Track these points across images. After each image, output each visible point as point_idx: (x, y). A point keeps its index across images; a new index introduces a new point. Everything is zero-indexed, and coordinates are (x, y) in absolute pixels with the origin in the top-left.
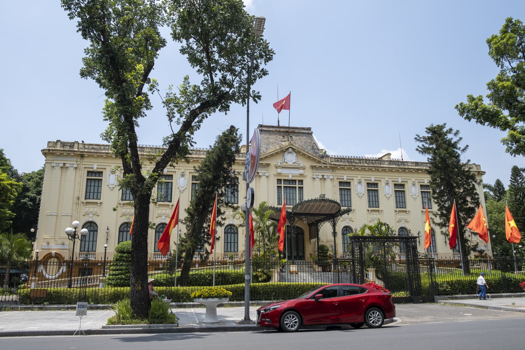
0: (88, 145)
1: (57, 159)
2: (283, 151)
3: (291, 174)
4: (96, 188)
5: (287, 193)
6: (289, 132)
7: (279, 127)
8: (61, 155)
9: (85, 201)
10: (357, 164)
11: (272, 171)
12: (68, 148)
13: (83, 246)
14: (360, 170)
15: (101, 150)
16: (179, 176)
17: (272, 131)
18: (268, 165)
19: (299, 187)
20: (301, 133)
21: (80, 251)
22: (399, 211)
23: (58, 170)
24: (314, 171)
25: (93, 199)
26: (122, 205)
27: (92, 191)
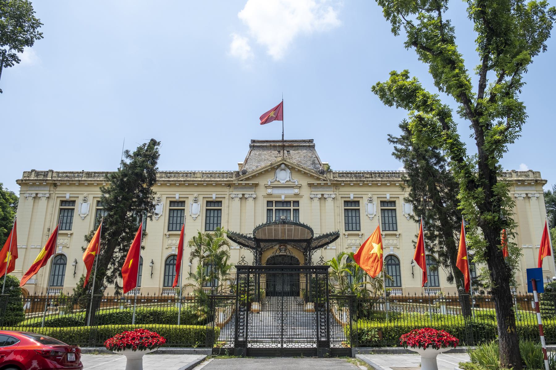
0: (62, 173)
1: (31, 189)
2: (273, 168)
3: (283, 195)
4: (216, 218)
5: (348, 217)
6: (284, 146)
7: (283, 141)
8: (34, 185)
9: (168, 233)
10: (367, 179)
11: (262, 192)
12: (41, 178)
13: (166, 281)
14: (370, 186)
15: (75, 177)
16: (81, 202)
17: (266, 146)
18: (256, 185)
19: (294, 210)
20: (301, 146)
21: (164, 286)
22: (349, 235)
23: (237, 202)
24: (312, 190)
25: (65, 230)
26: (346, 236)
27: (175, 222)
